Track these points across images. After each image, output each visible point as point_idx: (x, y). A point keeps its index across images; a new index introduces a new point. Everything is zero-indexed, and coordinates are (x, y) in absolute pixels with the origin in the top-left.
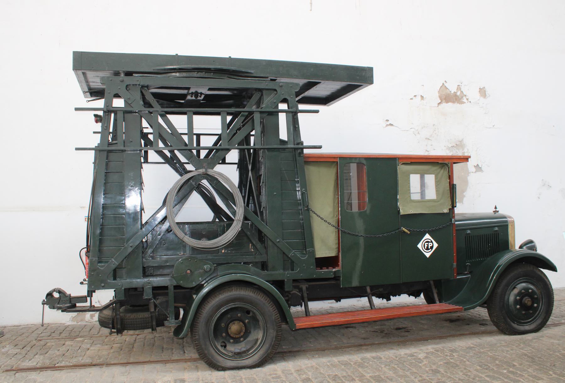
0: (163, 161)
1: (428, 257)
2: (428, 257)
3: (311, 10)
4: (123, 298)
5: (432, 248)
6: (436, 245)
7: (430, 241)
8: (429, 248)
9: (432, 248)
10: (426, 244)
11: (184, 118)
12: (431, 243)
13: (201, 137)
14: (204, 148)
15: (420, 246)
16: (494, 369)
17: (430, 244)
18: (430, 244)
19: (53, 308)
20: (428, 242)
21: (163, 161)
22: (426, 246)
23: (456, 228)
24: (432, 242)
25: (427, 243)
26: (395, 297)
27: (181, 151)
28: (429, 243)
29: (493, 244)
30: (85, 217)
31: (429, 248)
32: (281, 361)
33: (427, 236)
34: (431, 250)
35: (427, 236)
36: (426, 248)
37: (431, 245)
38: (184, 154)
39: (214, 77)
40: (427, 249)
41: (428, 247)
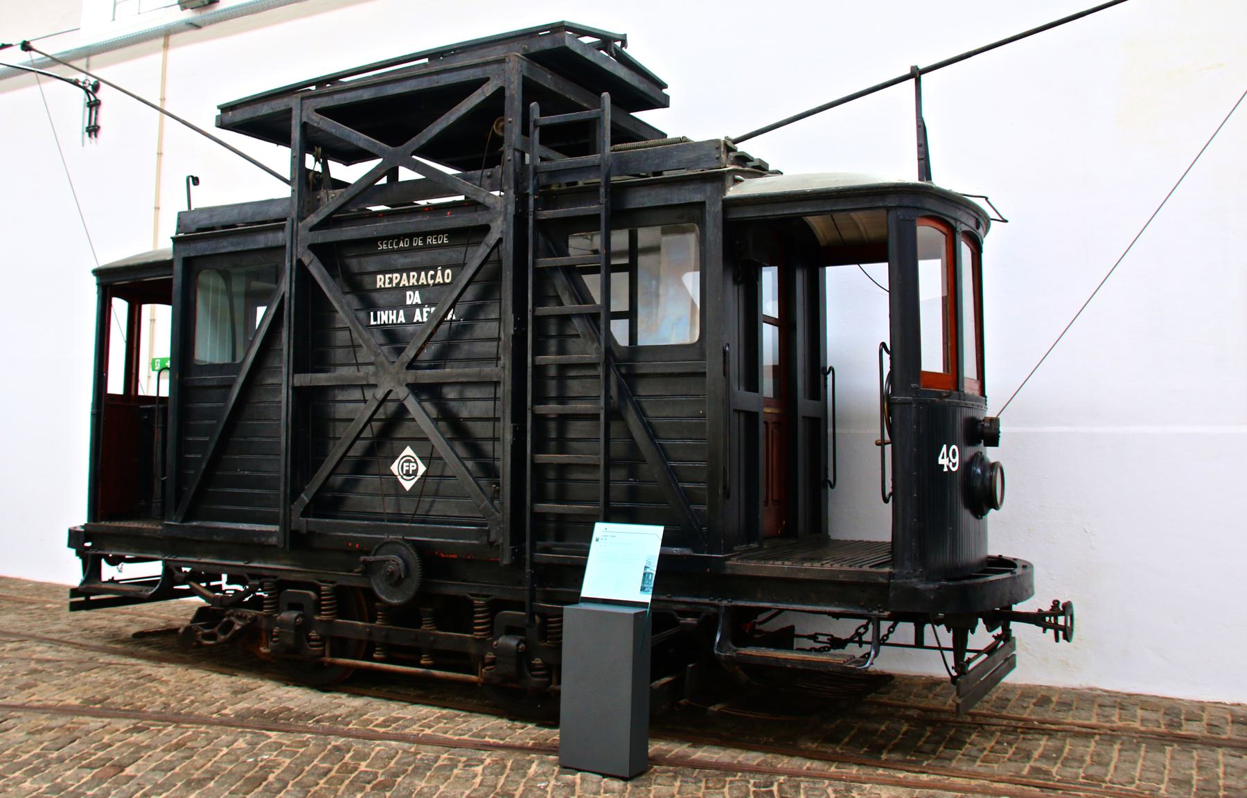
0: (469, 424)
1: (941, 371)
2: (941, 371)
3: (93, 130)
8: (411, 472)
10: (405, 464)
12: (414, 464)
21: (469, 424)
22: (405, 468)
23: (705, 445)
24: (415, 462)
25: (407, 464)
26: (74, 551)
27: (423, 436)
28: (411, 464)
31: (411, 472)
37: (415, 468)
38: (3, 581)
39: (856, 207)
40: (408, 474)
41: (408, 471)
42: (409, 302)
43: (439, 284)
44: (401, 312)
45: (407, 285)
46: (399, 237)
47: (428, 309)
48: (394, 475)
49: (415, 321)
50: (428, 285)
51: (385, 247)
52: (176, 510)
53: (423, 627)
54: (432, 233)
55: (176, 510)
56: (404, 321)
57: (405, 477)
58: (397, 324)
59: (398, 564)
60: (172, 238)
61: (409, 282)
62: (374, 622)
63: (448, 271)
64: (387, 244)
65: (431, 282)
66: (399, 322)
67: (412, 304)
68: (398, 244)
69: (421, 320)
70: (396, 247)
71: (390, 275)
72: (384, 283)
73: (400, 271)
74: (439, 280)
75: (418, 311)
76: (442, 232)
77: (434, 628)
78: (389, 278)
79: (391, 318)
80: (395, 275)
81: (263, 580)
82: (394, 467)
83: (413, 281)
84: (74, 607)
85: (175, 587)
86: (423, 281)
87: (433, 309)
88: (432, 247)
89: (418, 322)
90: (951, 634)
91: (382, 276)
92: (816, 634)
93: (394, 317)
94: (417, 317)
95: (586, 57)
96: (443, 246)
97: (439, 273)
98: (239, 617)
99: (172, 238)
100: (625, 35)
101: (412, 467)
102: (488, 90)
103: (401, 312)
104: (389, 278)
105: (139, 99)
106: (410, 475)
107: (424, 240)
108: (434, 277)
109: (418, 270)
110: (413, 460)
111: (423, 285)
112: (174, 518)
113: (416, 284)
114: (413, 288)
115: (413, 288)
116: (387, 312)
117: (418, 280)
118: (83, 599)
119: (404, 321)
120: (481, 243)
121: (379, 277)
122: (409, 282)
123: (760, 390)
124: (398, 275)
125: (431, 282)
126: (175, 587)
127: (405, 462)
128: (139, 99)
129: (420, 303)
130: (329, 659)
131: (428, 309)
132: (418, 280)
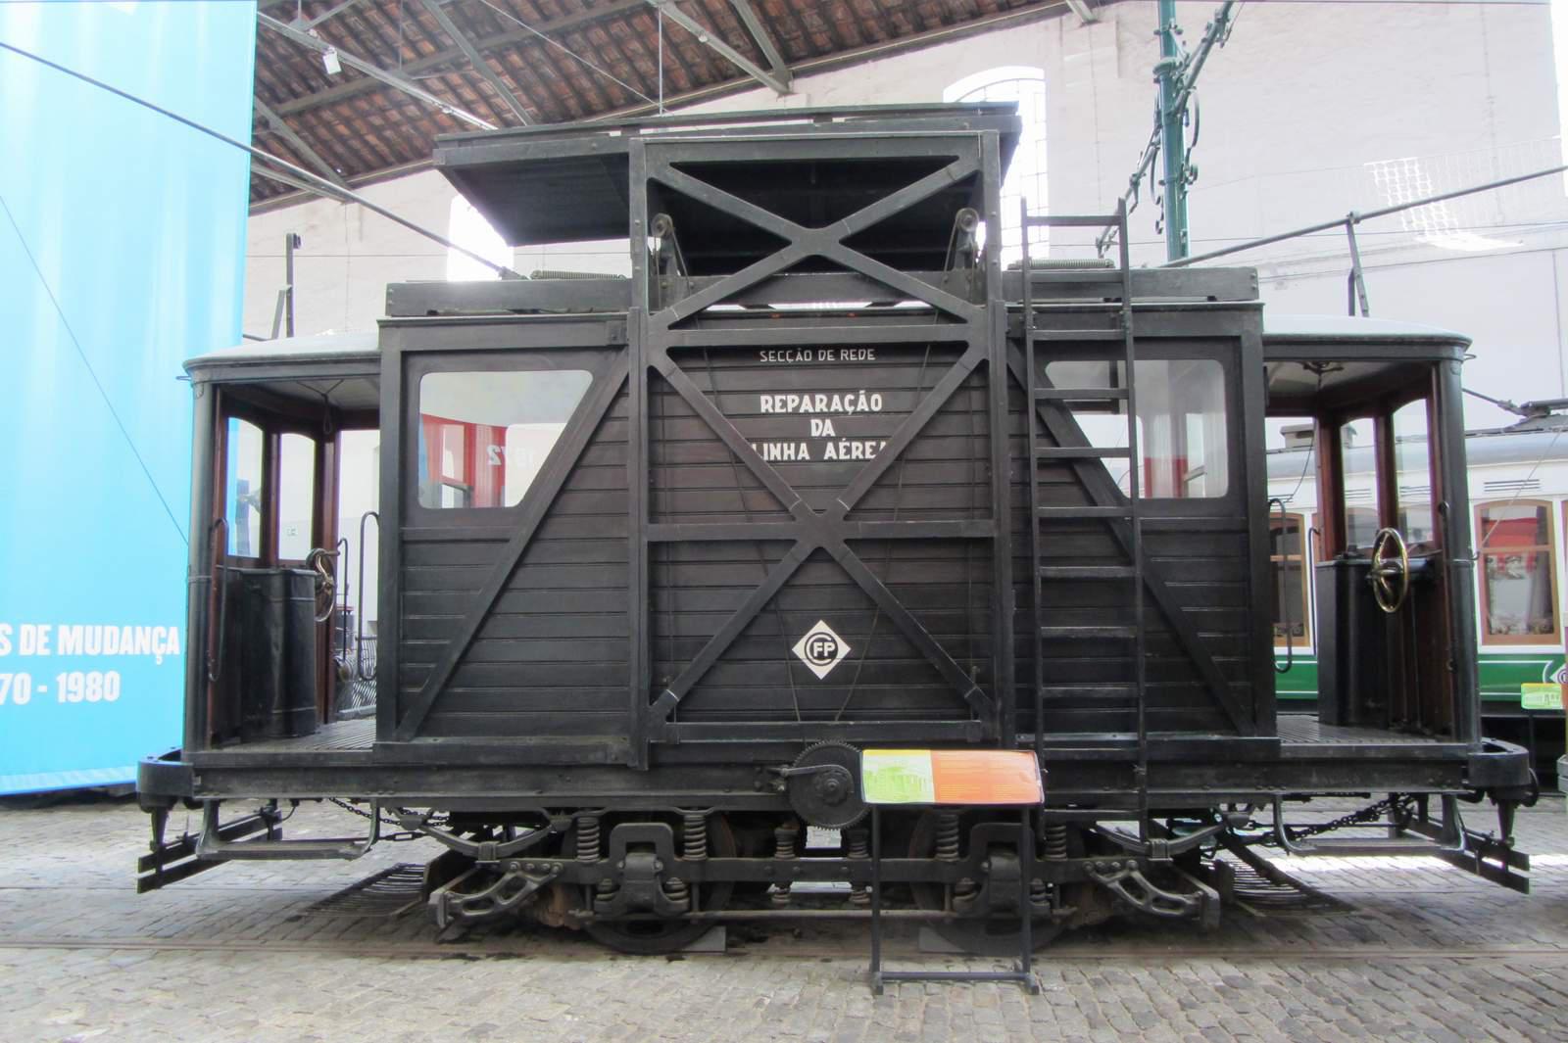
1: (1188, 415)
4: (1257, 809)
5: (833, 655)
6: (844, 650)
7: (830, 639)
8: (826, 654)
9: (833, 655)
11: (1118, 241)
13: (1030, 214)
14: (1116, 243)
15: (799, 649)
16: (1400, 179)
17: (830, 647)
18: (830, 647)
19: (1293, 535)
20: (824, 640)
22: (816, 650)
24: (833, 641)
25: (821, 644)
28: (826, 644)
29: (697, 833)
30: (1352, 312)
31: (826, 654)
32: (127, 806)
33: (821, 627)
34: (828, 661)
35: (821, 627)
36: (816, 655)
40: (821, 656)
42: (815, 433)
43: (863, 412)
44: (803, 446)
45: (811, 410)
46: (794, 349)
47: (848, 444)
48: (799, 659)
49: (826, 458)
50: (845, 413)
51: (772, 359)
52: (398, 723)
53: (779, 855)
54: (848, 347)
55: (398, 723)
56: (808, 458)
57: (816, 661)
58: (796, 461)
59: (844, 775)
60: (379, 322)
61: (814, 408)
62: (771, 854)
63: (876, 396)
64: (775, 355)
65: (850, 409)
66: (799, 458)
67: (820, 436)
68: (794, 356)
69: (835, 457)
70: (790, 361)
71: (784, 397)
72: (773, 407)
73: (800, 392)
74: (862, 405)
75: (830, 446)
76: (866, 346)
77: (866, 855)
78: (781, 400)
79: (786, 452)
80: (790, 397)
81: (576, 814)
82: (799, 649)
83: (821, 407)
84: (146, 885)
85: (1176, 819)
86: (836, 405)
87: (883, 444)
88: (848, 365)
89: (831, 460)
90: (1497, 807)
91: (769, 398)
92: (412, 839)
93: (792, 451)
94: (830, 452)
95: (944, 169)
96: (866, 365)
97: (862, 398)
98: (535, 871)
99: (379, 322)
100: (252, 213)
101: (828, 648)
102: (956, 172)
103: (803, 446)
104: (781, 400)
105: (171, 115)
106: (823, 658)
107: (815, 355)
108: (854, 403)
109: (829, 392)
110: (830, 639)
111: (837, 413)
112: (394, 735)
113: (825, 410)
114: (822, 415)
115: (822, 415)
116: (779, 445)
117: (829, 405)
118: (165, 867)
119: (808, 458)
120: (952, 364)
121: (763, 398)
122: (814, 408)
123: (1550, 540)
124: (796, 398)
125: (850, 409)
126: (1176, 819)
127: (815, 641)
128: (171, 115)
129: (833, 434)
130: (701, 914)
131: (848, 444)
132: (829, 405)
